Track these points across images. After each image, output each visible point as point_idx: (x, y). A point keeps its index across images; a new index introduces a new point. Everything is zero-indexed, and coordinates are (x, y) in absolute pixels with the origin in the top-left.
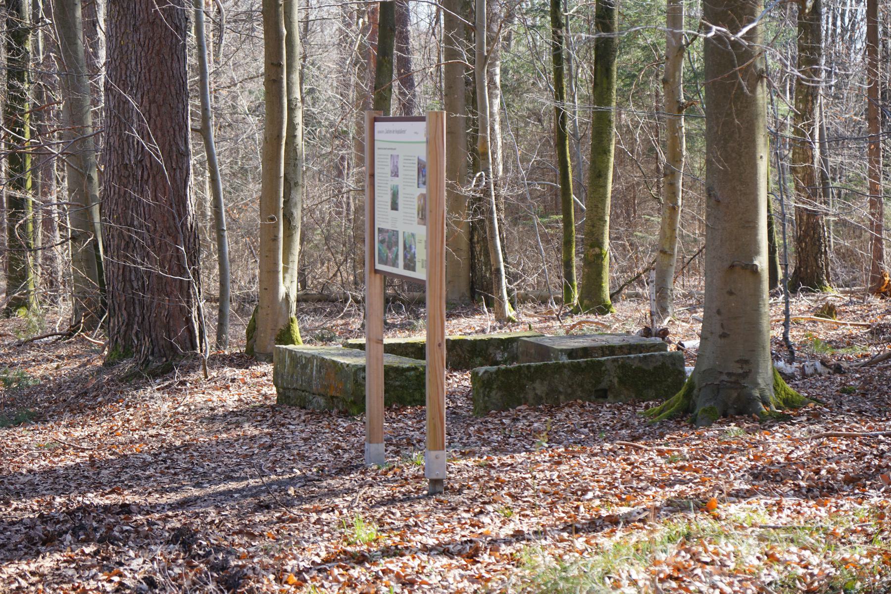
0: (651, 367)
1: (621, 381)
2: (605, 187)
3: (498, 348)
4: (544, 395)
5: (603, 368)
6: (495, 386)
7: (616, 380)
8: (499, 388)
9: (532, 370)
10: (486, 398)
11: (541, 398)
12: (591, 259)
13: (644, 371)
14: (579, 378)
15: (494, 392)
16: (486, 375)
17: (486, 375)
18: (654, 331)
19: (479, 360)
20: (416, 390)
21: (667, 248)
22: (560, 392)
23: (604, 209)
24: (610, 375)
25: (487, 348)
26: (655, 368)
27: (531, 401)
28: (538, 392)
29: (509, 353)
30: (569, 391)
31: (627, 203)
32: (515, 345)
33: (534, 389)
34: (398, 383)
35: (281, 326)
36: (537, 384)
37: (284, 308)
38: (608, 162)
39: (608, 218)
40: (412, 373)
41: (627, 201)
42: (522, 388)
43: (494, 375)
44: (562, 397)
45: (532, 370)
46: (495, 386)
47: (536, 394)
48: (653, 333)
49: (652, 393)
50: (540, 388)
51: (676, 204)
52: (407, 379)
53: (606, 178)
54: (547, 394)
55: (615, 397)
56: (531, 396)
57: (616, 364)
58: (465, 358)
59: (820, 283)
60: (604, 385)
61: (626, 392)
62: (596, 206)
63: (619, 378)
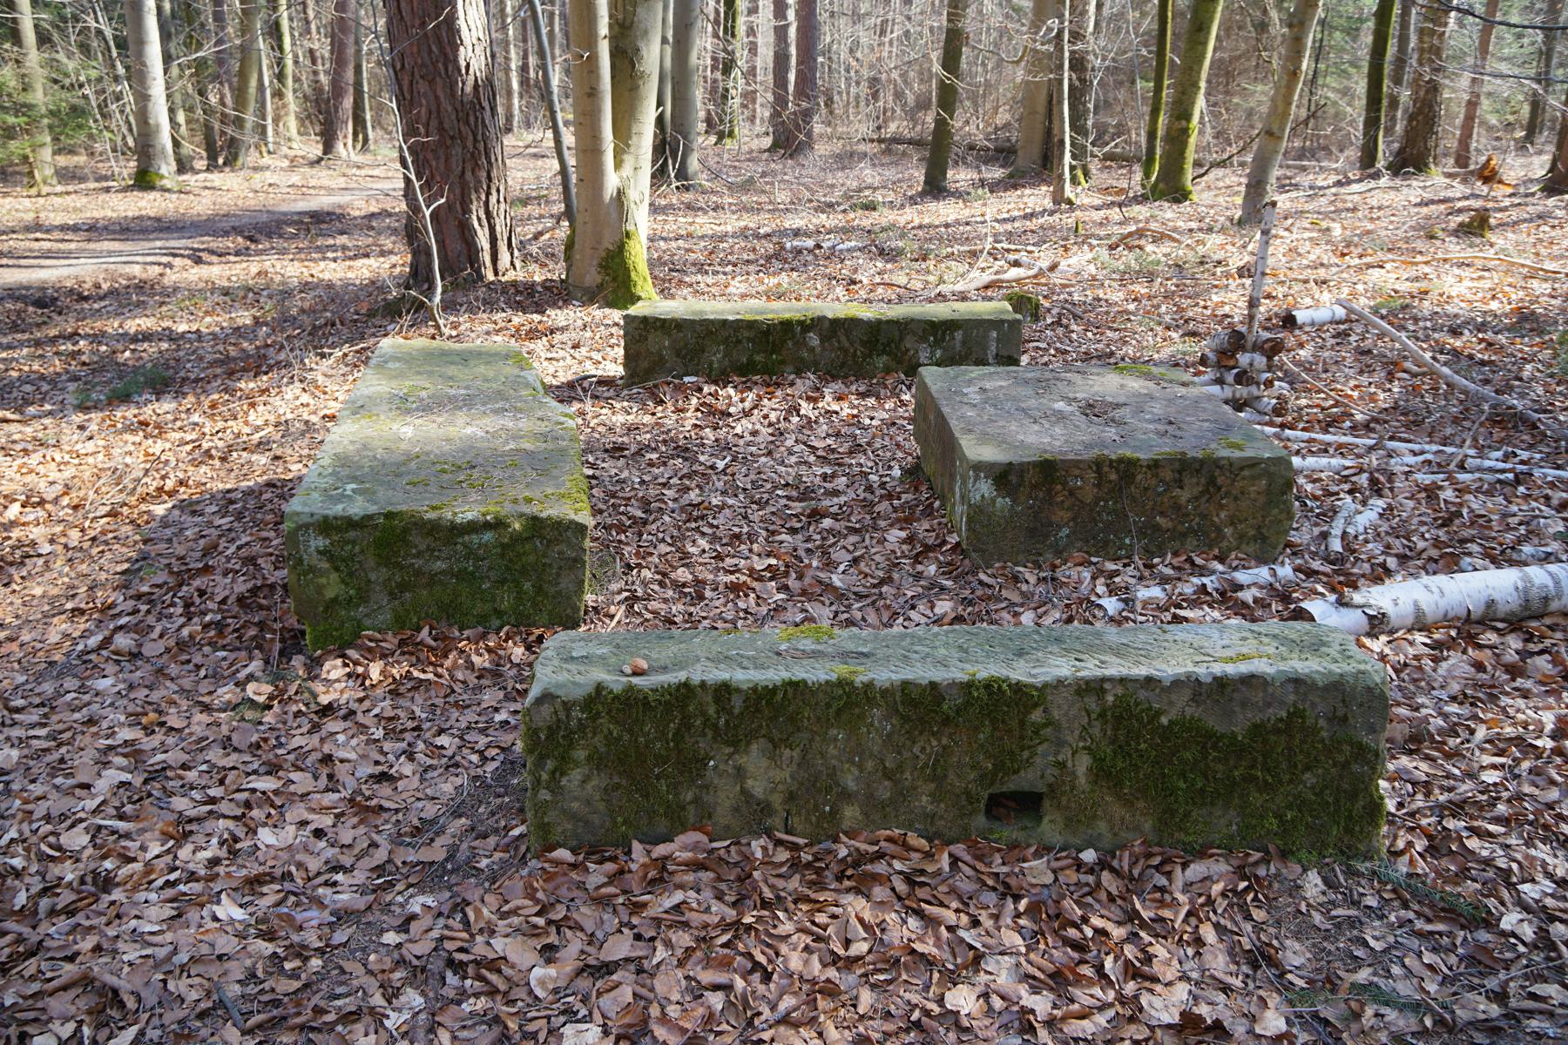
0: (1239, 727)
1: (1102, 773)
2: (1205, 44)
3: (923, 339)
4: (777, 800)
5: (1036, 716)
6: (580, 754)
7: (1083, 764)
8: (597, 762)
9: (737, 703)
10: (545, 795)
11: (766, 809)
12: (1174, 134)
13: (1208, 739)
14: (927, 747)
15: (576, 775)
16: (546, 710)
17: (546, 710)
18: (1251, 339)
19: (881, 361)
20: (502, 582)
21: (1275, 129)
22: (846, 796)
23: (1199, 73)
24: (1060, 743)
25: (901, 339)
26: (1257, 730)
27: (723, 816)
28: (757, 787)
29: (944, 349)
30: (884, 791)
31: (1225, 73)
32: (959, 335)
33: (740, 773)
34: (440, 565)
35: (608, 243)
36: (754, 759)
37: (614, 215)
38: (1214, 12)
39: (1203, 84)
40: (488, 536)
41: (1228, 73)
42: (693, 766)
43: (576, 713)
44: (851, 813)
45: (737, 703)
46: (580, 754)
47: (744, 791)
48: (1249, 345)
49: (1226, 821)
50: (764, 771)
51: (1299, 68)
52: (470, 553)
53: (1208, 33)
54: (791, 797)
55: (1070, 823)
56: (724, 798)
57: (1091, 702)
58: (855, 354)
59: (1426, 165)
60: (1026, 780)
61: (1118, 811)
62: (1191, 69)
63: (1098, 760)
